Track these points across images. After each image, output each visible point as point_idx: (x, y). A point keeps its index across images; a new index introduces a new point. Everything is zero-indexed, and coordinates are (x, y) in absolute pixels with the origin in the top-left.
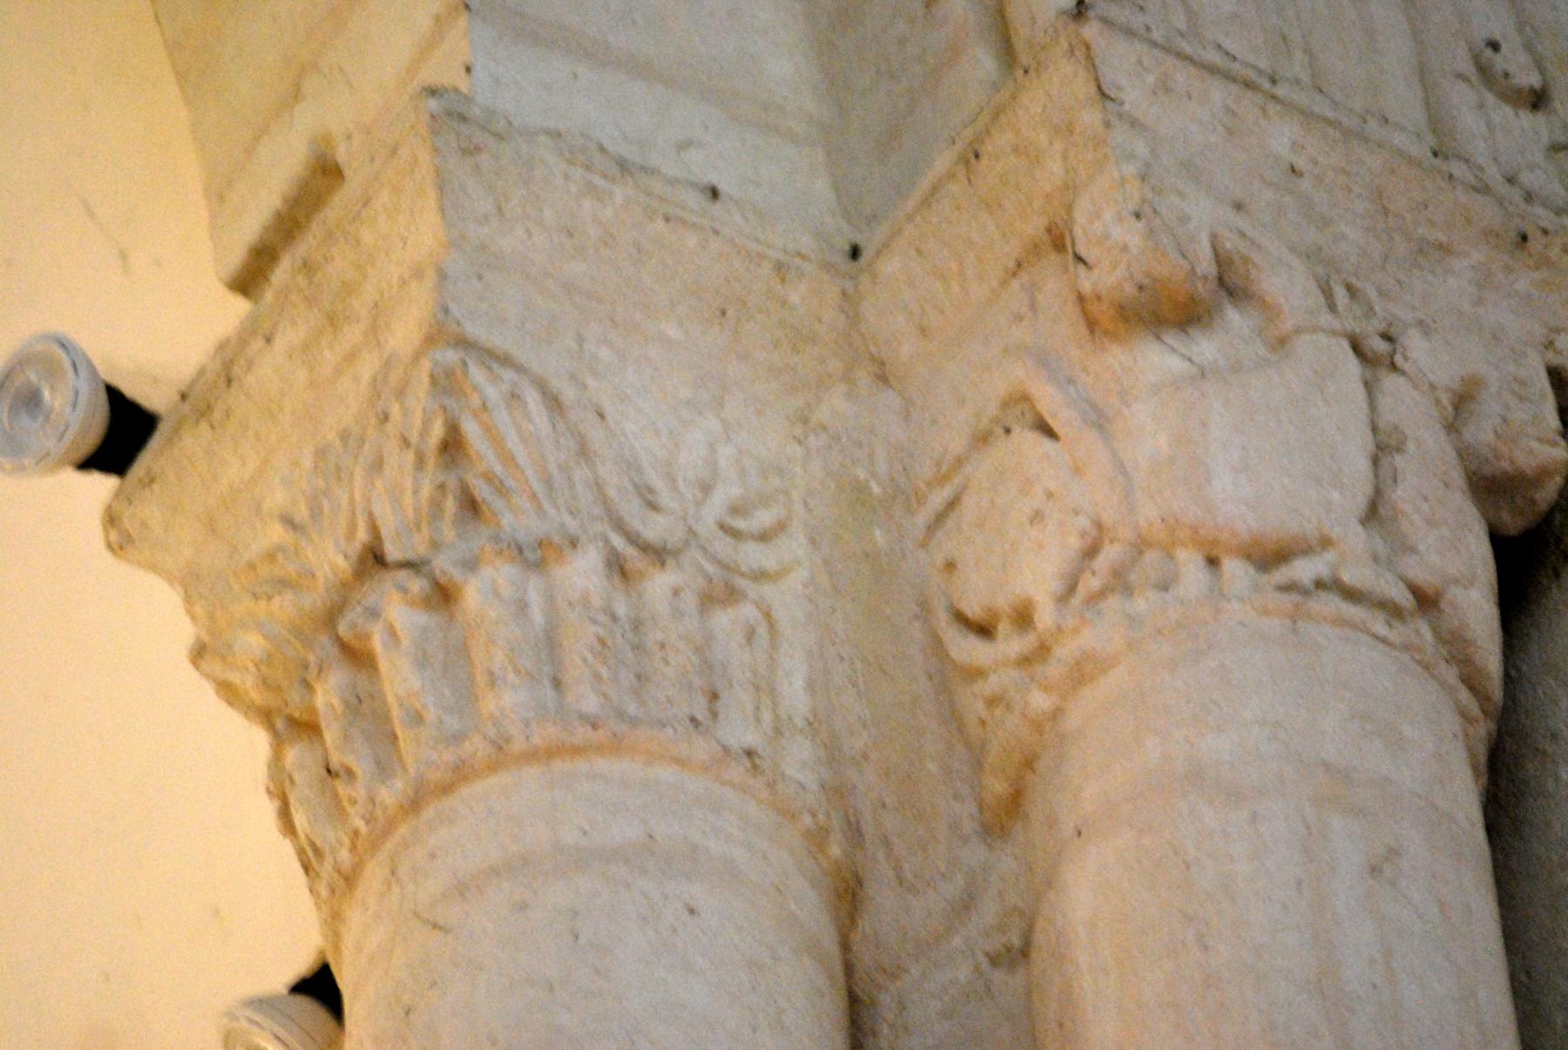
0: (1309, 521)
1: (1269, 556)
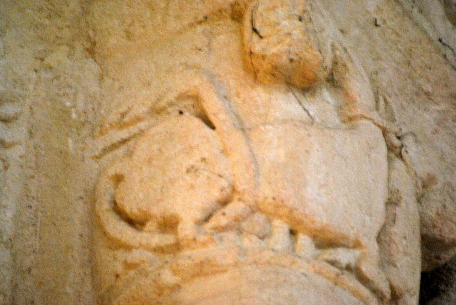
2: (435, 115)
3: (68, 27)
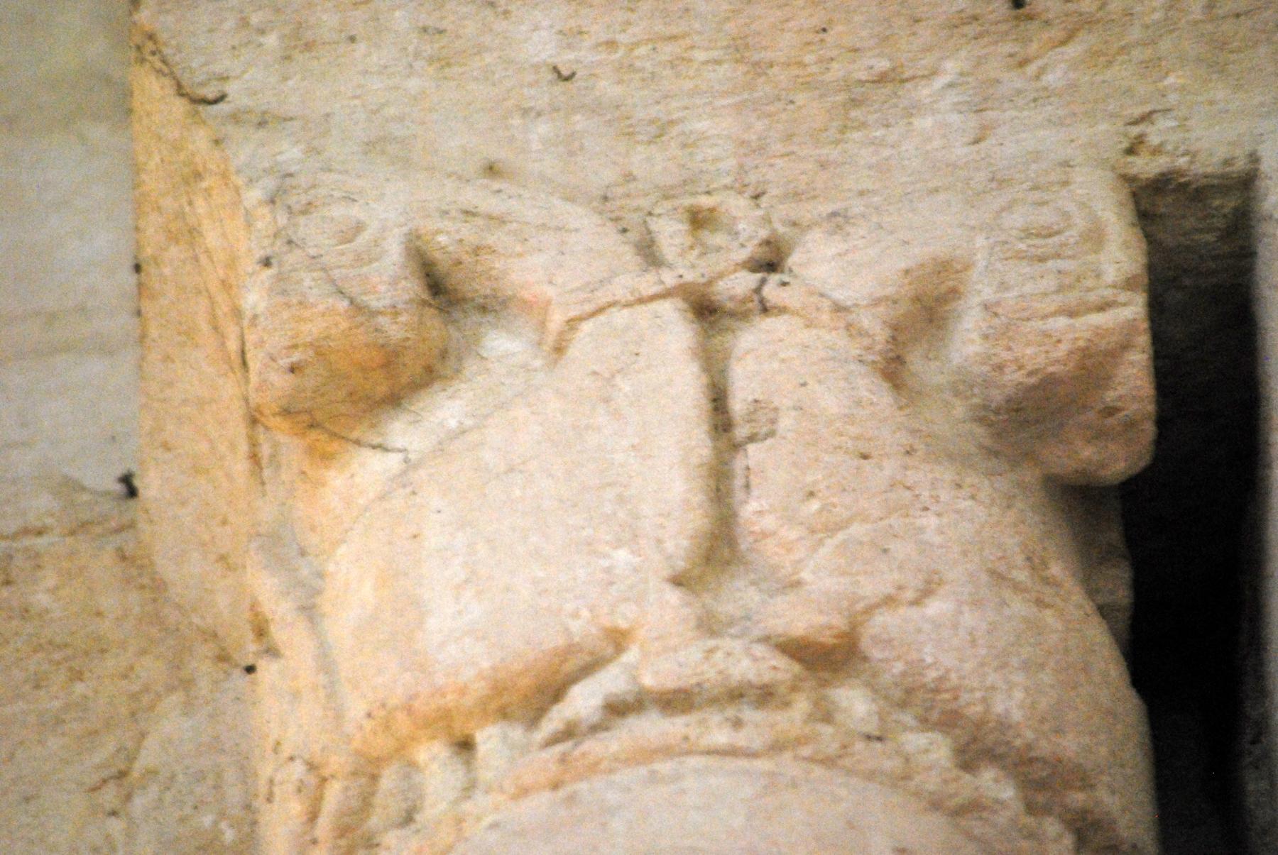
0: (575, 615)
1: (534, 695)
2: (952, 97)
3: (143, 652)
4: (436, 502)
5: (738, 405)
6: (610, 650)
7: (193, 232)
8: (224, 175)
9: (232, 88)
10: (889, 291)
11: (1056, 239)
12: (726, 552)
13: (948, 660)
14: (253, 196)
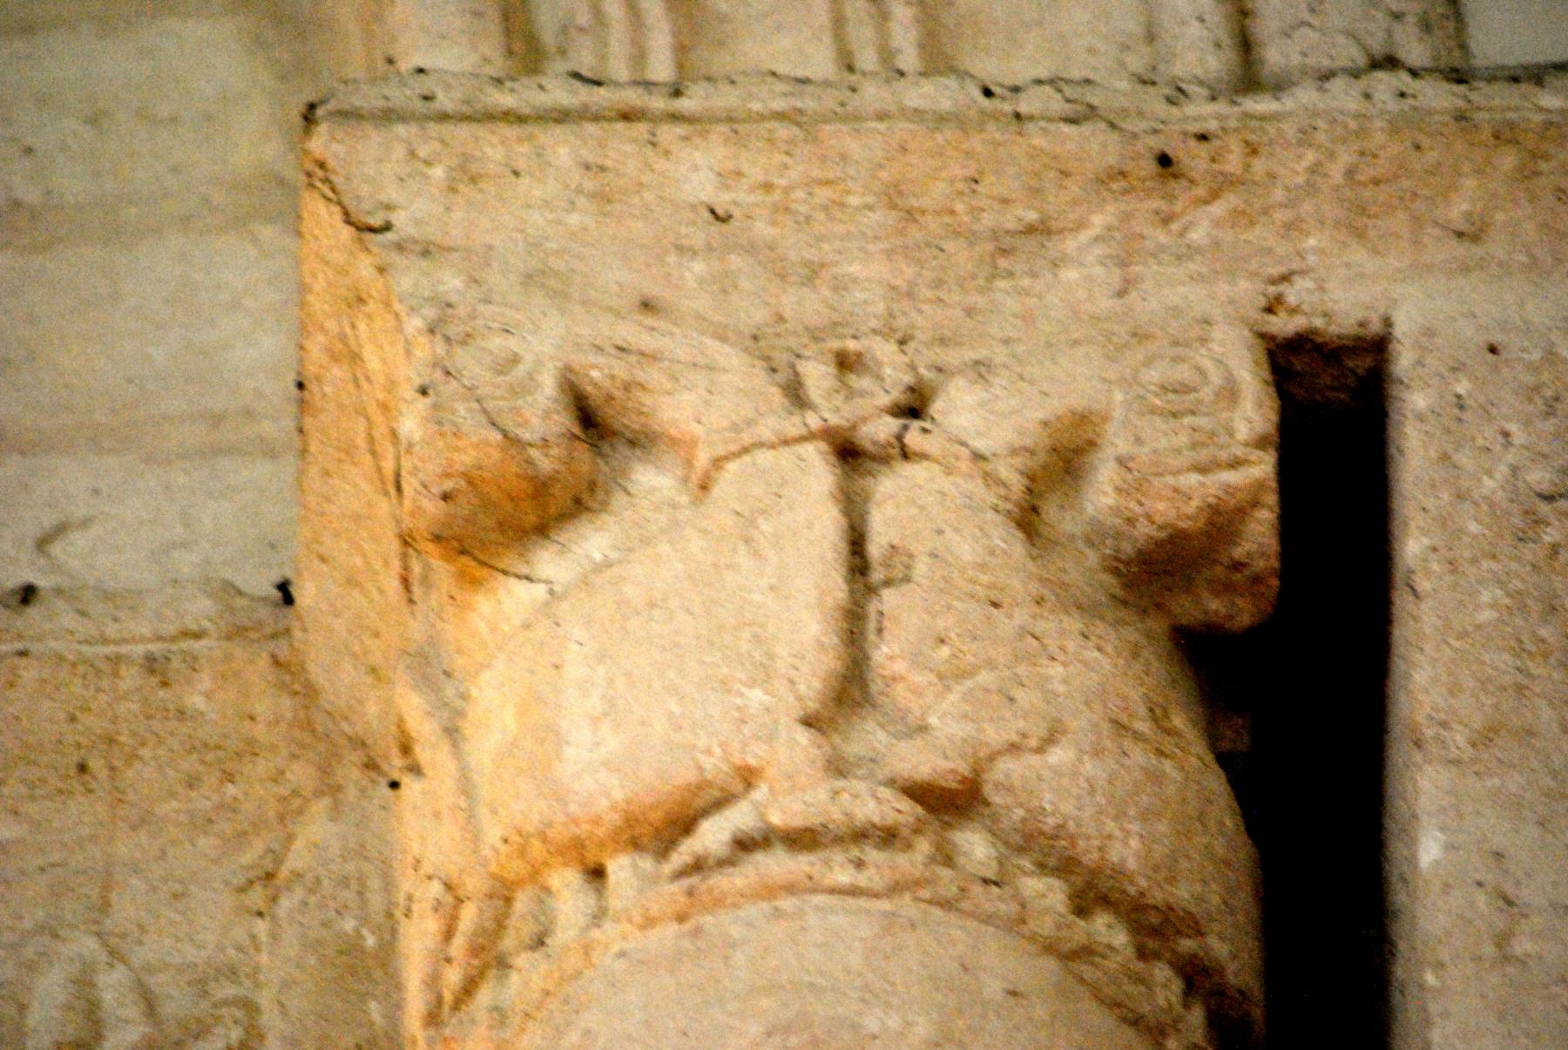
0: (709, 752)
1: (665, 828)
2: (1099, 250)
4: (579, 633)
5: (875, 549)
6: (740, 787)
7: (355, 358)
8: (387, 304)
9: (398, 218)
10: (1028, 442)
11: (1192, 396)
12: (857, 694)
13: (1068, 808)
14: (414, 324)
